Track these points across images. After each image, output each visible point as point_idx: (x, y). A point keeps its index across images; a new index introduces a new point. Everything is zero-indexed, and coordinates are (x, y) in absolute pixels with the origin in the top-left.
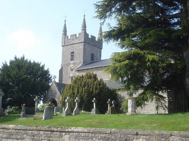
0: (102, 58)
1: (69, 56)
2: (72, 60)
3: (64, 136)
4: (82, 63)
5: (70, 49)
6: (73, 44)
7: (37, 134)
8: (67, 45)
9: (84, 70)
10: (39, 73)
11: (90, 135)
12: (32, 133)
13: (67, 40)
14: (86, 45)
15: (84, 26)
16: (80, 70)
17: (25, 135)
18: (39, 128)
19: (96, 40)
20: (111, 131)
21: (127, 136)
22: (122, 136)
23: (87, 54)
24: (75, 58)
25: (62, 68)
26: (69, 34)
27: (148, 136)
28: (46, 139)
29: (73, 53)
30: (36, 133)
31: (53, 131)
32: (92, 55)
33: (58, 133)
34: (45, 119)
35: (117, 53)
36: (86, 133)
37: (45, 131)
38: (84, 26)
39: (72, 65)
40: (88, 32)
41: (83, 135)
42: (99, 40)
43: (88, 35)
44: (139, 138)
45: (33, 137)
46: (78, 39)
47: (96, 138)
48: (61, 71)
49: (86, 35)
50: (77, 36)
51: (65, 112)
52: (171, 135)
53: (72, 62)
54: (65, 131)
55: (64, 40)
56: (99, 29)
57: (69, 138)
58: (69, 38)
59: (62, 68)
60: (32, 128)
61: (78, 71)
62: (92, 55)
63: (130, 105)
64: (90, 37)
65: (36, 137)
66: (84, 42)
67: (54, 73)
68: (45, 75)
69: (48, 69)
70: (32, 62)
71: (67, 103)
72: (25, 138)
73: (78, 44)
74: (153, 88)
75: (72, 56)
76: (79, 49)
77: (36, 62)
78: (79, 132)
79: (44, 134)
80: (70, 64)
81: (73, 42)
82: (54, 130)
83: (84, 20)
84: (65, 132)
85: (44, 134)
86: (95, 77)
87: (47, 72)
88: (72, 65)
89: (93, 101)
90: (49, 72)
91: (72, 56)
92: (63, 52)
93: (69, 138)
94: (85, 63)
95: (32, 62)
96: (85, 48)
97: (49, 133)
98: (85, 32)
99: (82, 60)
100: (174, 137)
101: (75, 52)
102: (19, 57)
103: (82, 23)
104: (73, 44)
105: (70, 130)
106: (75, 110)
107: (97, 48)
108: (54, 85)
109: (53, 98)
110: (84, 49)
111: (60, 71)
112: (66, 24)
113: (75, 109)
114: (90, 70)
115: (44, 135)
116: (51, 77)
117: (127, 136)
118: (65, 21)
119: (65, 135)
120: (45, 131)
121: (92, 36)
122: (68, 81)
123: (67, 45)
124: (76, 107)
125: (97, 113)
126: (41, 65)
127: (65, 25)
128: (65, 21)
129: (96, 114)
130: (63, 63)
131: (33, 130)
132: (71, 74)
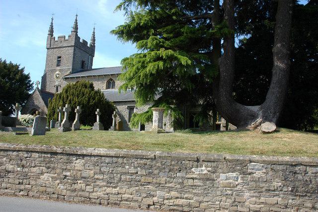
0: (93, 68)
2: (58, 65)
3: (75, 162)
4: (71, 70)
6: (61, 47)
7: (26, 158)
8: (53, 48)
9: (74, 78)
10: (18, 77)
11: (120, 160)
12: (18, 156)
13: (52, 44)
14: (77, 50)
15: (76, 28)
16: (68, 78)
17: (5, 159)
18: (30, 147)
20: (155, 156)
21: (181, 163)
22: (173, 163)
25: (46, 74)
26: (56, 35)
27: (216, 163)
28: (43, 165)
29: (60, 57)
30: (26, 155)
31: (56, 153)
32: (83, 62)
33: (65, 157)
34: (35, 134)
35: (133, 55)
36: (113, 157)
37: (42, 152)
39: (57, 72)
41: (107, 160)
43: (79, 38)
44: (201, 166)
45: (19, 162)
47: (130, 165)
48: (44, 78)
49: (77, 38)
50: (67, 38)
51: (117, 123)
52: (251, 162)
53: (58, 68)
54: (76, 153)
55: (49, 42)
56: (93, 33)
57: (84, 165)
58: (56, 39)
59: (46, 74)
60: (18, 147)
61: (66, 78)
62: (83, 62)
63: (157, 119)
64: (81, 41)
65: (25, 162)
66: (74, 46)
67: (35, 78)
68: (24, 80)
70: (8, 62)
71: (77, 114)
72: (5, 163)
74: (165, 100)
75: (59, 62)
76: (68, 54)
77: (14, 63)
78: (101, 156)
79: (39, 157)
80: (55, 71)
81: (60, 45)
82: (58, 152)
83: (76, 20)
84: (77, 155)
85: (39, 157)
86: (92, 86)
87: (27, 77)
88: (57, 72)
89: (96, 113)
91: (59, 62)
93: (84, 165)
94: (74, 71)
96: (75, 53)
97: (49, 155)
98: (77, 35)
99: (71, 67)
100: (254, 163)
103: (73, 24)
104: (61, 47)
105: (85, 152)
106: (74, 123)
107: (88, 55)
108: (37, 92)
110: (74, 54)
113: (75, 121)
115: (40, 159)
116: (33, 83)
117: (181, 163)
118: (52, 19)
119: (76, 160)
120: (42, 152)
121: (84, 41)
122: (51, 89)
123: (53, 48)
124: (76, 119)
125: (101, 129)
126: (20, 68)
128: (52, 19)
129: (175, 130)
130: (47, 69)
131: (19, 151)
132: (58, 84)
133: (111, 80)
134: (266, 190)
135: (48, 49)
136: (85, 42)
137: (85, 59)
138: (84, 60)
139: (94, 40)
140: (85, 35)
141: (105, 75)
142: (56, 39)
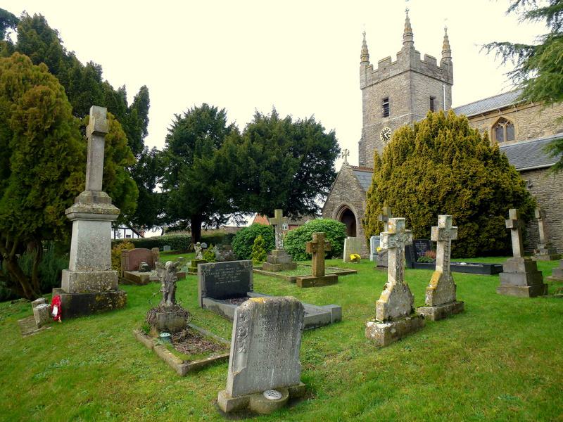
1: (379, 109)
2: (386, 114)
5: (379, 92)
15: (409, 34)
19: (438, 65)
23: (420, 98)
24: (391, 109)
26: (374, 62)
29: (386, 100)
38: (409, 34)
40: (417, 47)
42: (443, 63)
46: (396, 66)
50: (394, 59)
53: (386, 120)
56: (443, 39)
64: (422, 58)
69: (274, 111)
73: (396, 78)
89: (434, 236)
90: (125, 94)
92: (364, 101)
95: (32, 16)
101: (391, 96)
102: (267, 113)
106: (387, 292)
107: (441, 84)
109: (344, 206)
111: (360, 143)
112: (366, 40)
114: (483, 117)
118: (364, 34)
121: (427, 57)
127: (364, 41)
130: (366, 125)
133: (502, 120)
134: (54, 199)
135: (362, 89)
136: (430, 60)
137: (436, 94)
138: (433, 95)
139: (447, 50)
140: (428, 47)
141: (485, 114)
142: (376, 67)
